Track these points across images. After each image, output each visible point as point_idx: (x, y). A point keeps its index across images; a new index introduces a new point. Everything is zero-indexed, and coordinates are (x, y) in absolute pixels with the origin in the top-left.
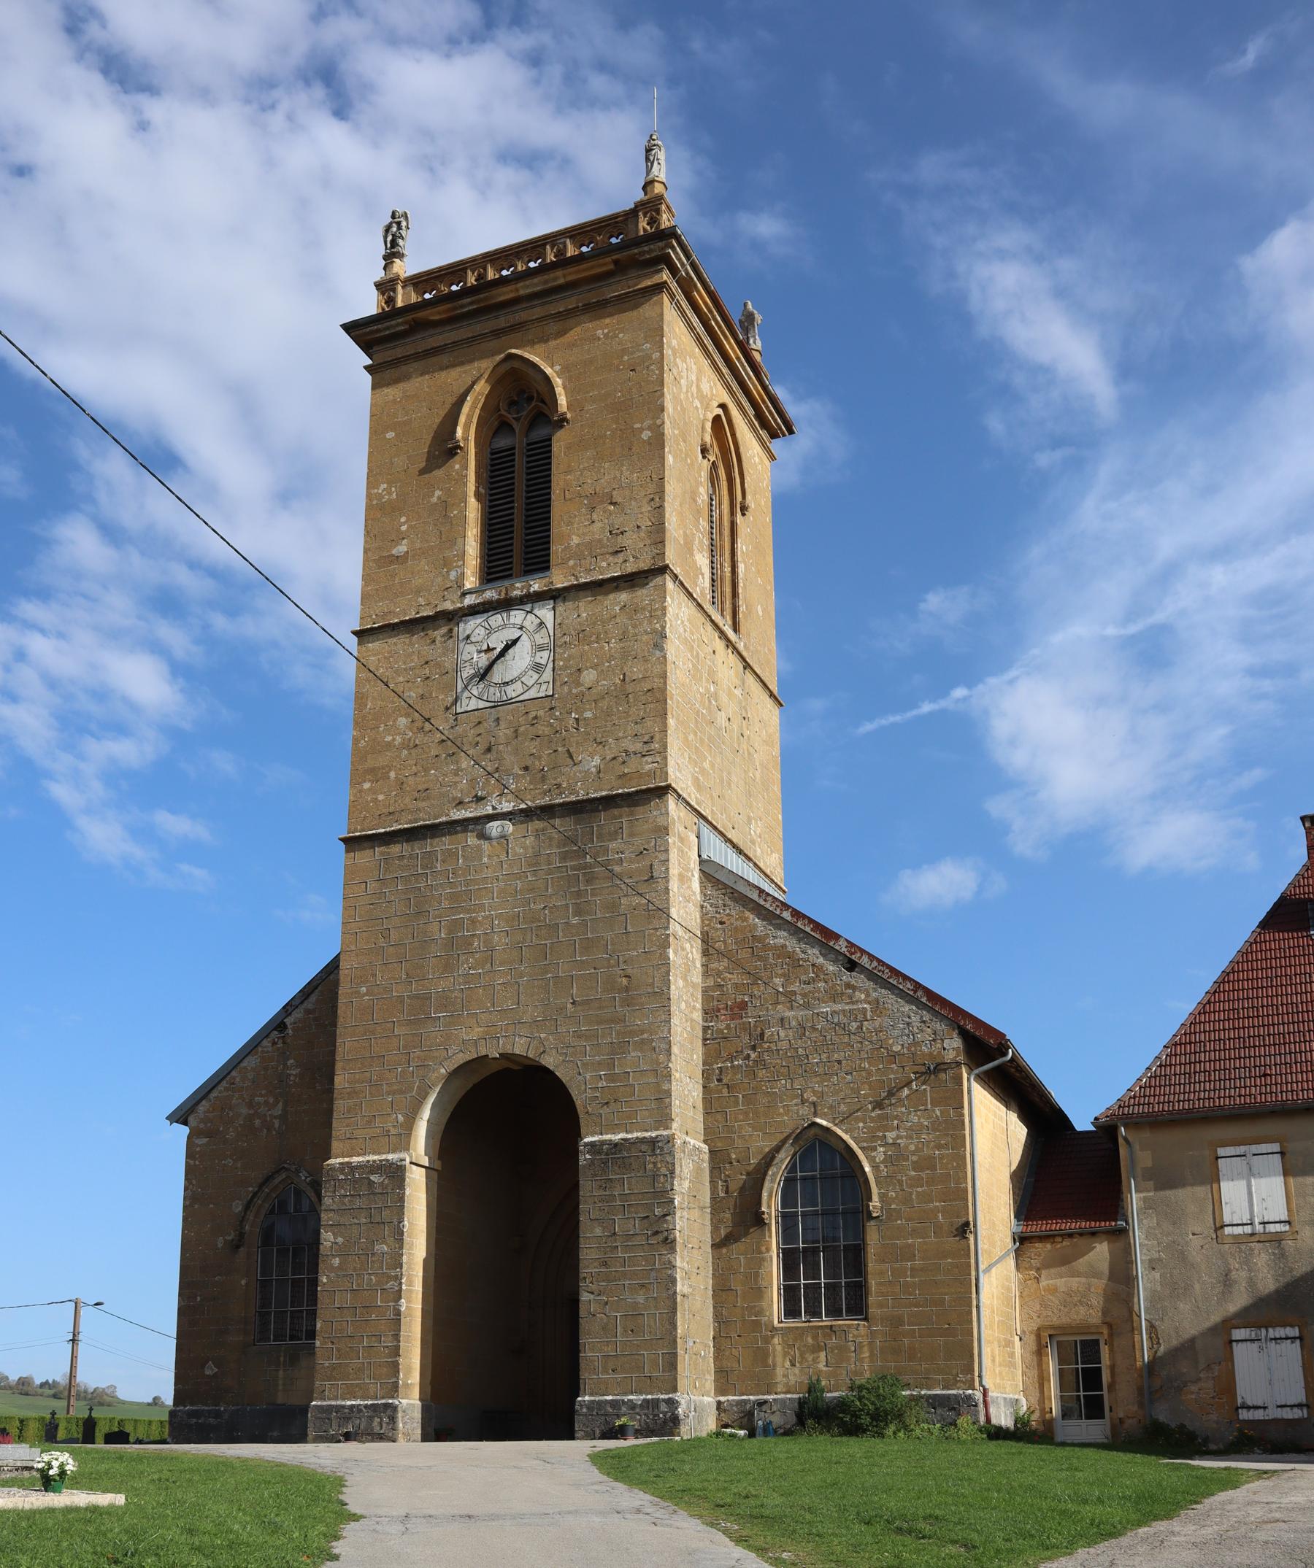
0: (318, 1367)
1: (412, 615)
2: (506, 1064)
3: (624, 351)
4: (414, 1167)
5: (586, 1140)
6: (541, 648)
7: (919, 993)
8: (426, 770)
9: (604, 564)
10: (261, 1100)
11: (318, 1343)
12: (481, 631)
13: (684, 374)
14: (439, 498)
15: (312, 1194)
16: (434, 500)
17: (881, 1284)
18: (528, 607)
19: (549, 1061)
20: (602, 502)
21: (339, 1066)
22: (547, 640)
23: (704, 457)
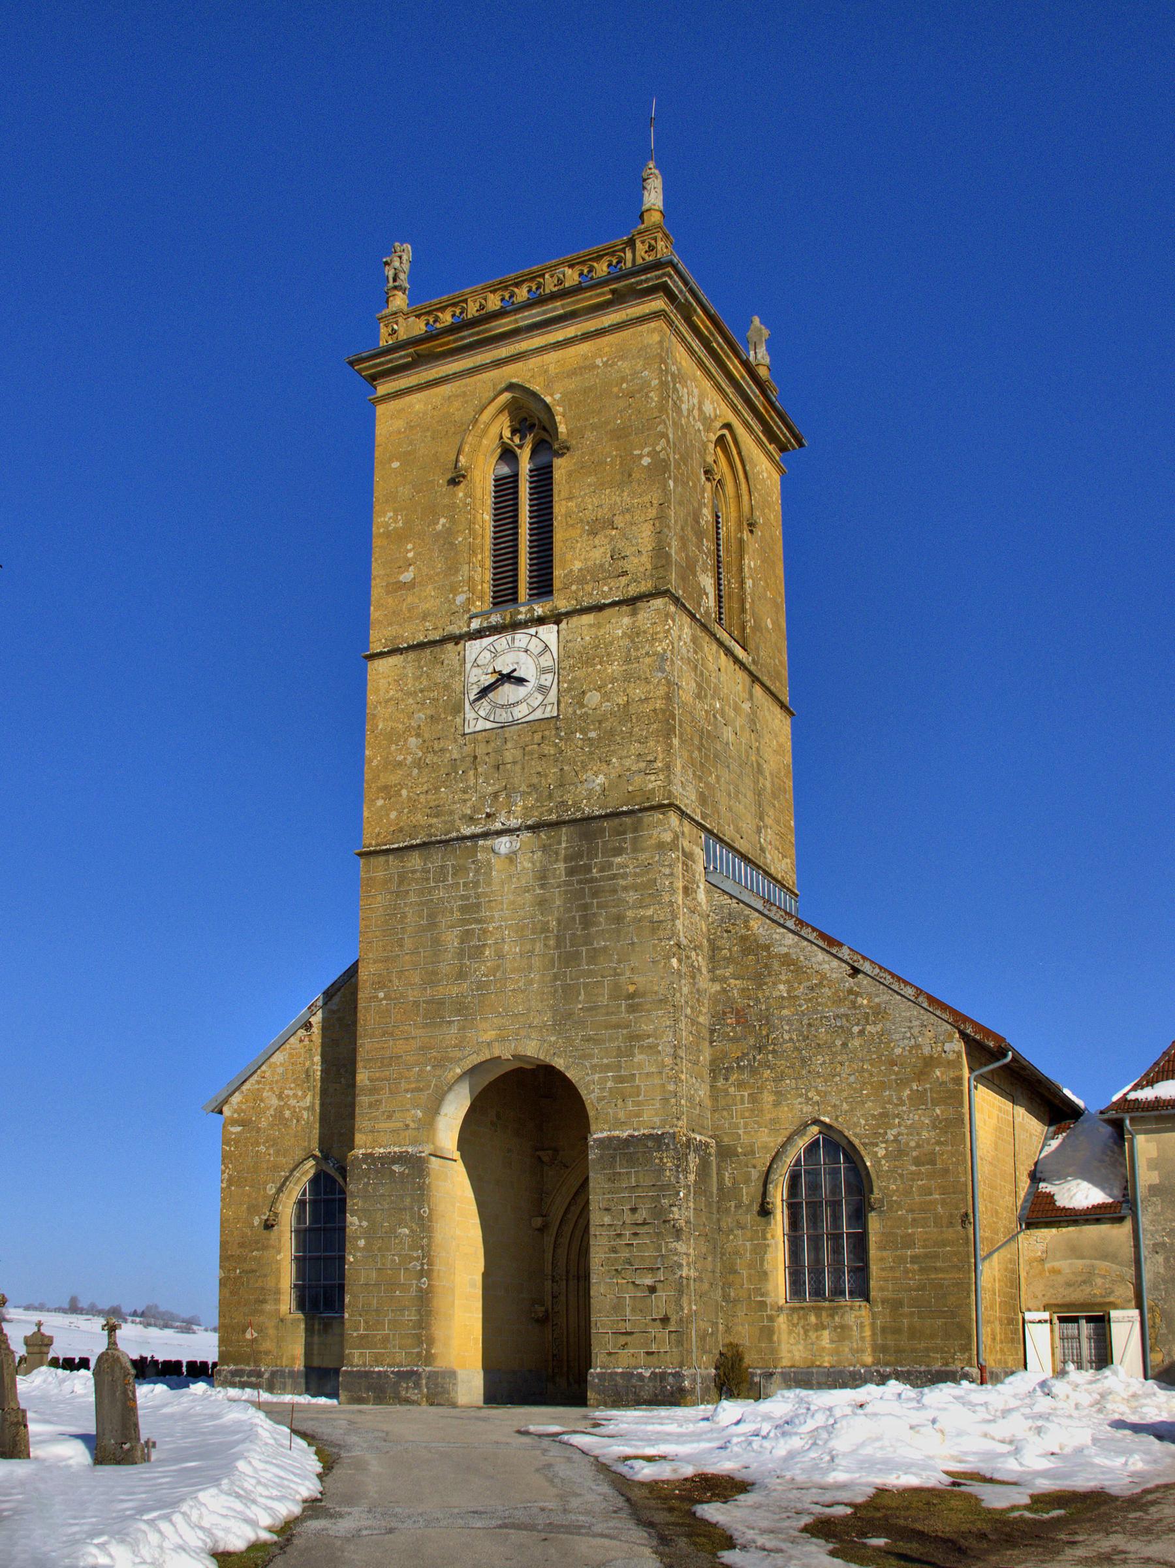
0: (347, 1337)
1: (421, 638)
2: (518, 1065)
3: (623, 379)
4: (433, 1159)
5: (595, 1136)
6: (544, 671)
7: (920, 999)
8: (437, 789)
9: (606, 589)
10: (291, 1093)
11: (346, 1315)
12: (487, 655)
13: (685, 398)
14: (444, 525)
15: (340, 1180)
16: (439, 527)
17: (883, 1269)
18: (532, 631)
19: (559, 1063)
20: (603, 528)
21: (360, 1064)
22: (550, 663)
23: (708, 479)
